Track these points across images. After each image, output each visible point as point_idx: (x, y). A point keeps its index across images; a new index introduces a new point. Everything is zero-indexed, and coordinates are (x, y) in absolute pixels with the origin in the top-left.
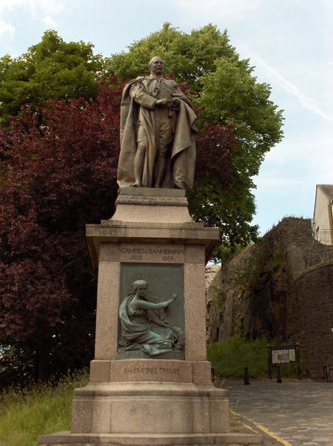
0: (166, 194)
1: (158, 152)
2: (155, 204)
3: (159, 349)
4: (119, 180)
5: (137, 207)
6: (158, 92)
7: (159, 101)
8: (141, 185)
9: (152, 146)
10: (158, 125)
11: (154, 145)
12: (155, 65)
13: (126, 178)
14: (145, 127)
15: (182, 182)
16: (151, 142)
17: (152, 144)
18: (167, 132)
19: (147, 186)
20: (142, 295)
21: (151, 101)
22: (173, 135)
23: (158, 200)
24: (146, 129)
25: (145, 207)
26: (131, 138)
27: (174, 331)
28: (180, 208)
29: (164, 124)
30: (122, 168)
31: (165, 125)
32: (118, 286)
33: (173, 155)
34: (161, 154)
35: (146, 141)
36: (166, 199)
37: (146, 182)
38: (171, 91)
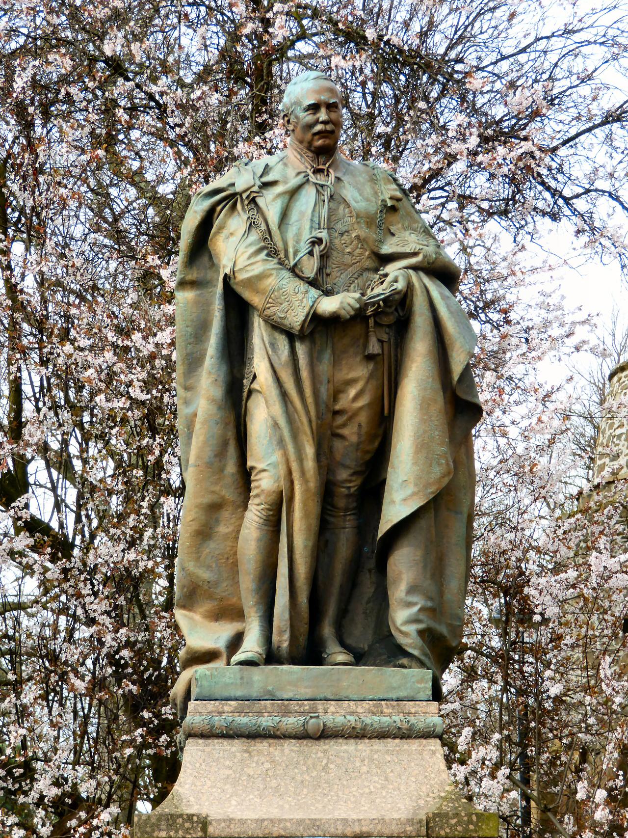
0: (346, 687)
1: (327, 492)
2: (325, 734)
4: (184, 607)
5: (263, 746)
6: (324, 257)
7: (329, 305)
8: (271, 657)
9: (306, 491)
11: (312, 485)
12: (309, 118)
14: (277, 409)
15: (421, 633)
16: (303, 473)
17: (305, 481)
18: (363, 418)
19: (294, 660)
20: (199, 591)
21: (298, 303)
23: (335, 715)
24: (282, 422)
25: (290, 747)
26: (225, 444)
28: (414, 745)
30: (191, 566)
31: (352, 392)
33: (384, 526)
34: (341, 503)
35: (282, 470)
36: (363, 714)
37: (286, 636)
38: (372, 235)
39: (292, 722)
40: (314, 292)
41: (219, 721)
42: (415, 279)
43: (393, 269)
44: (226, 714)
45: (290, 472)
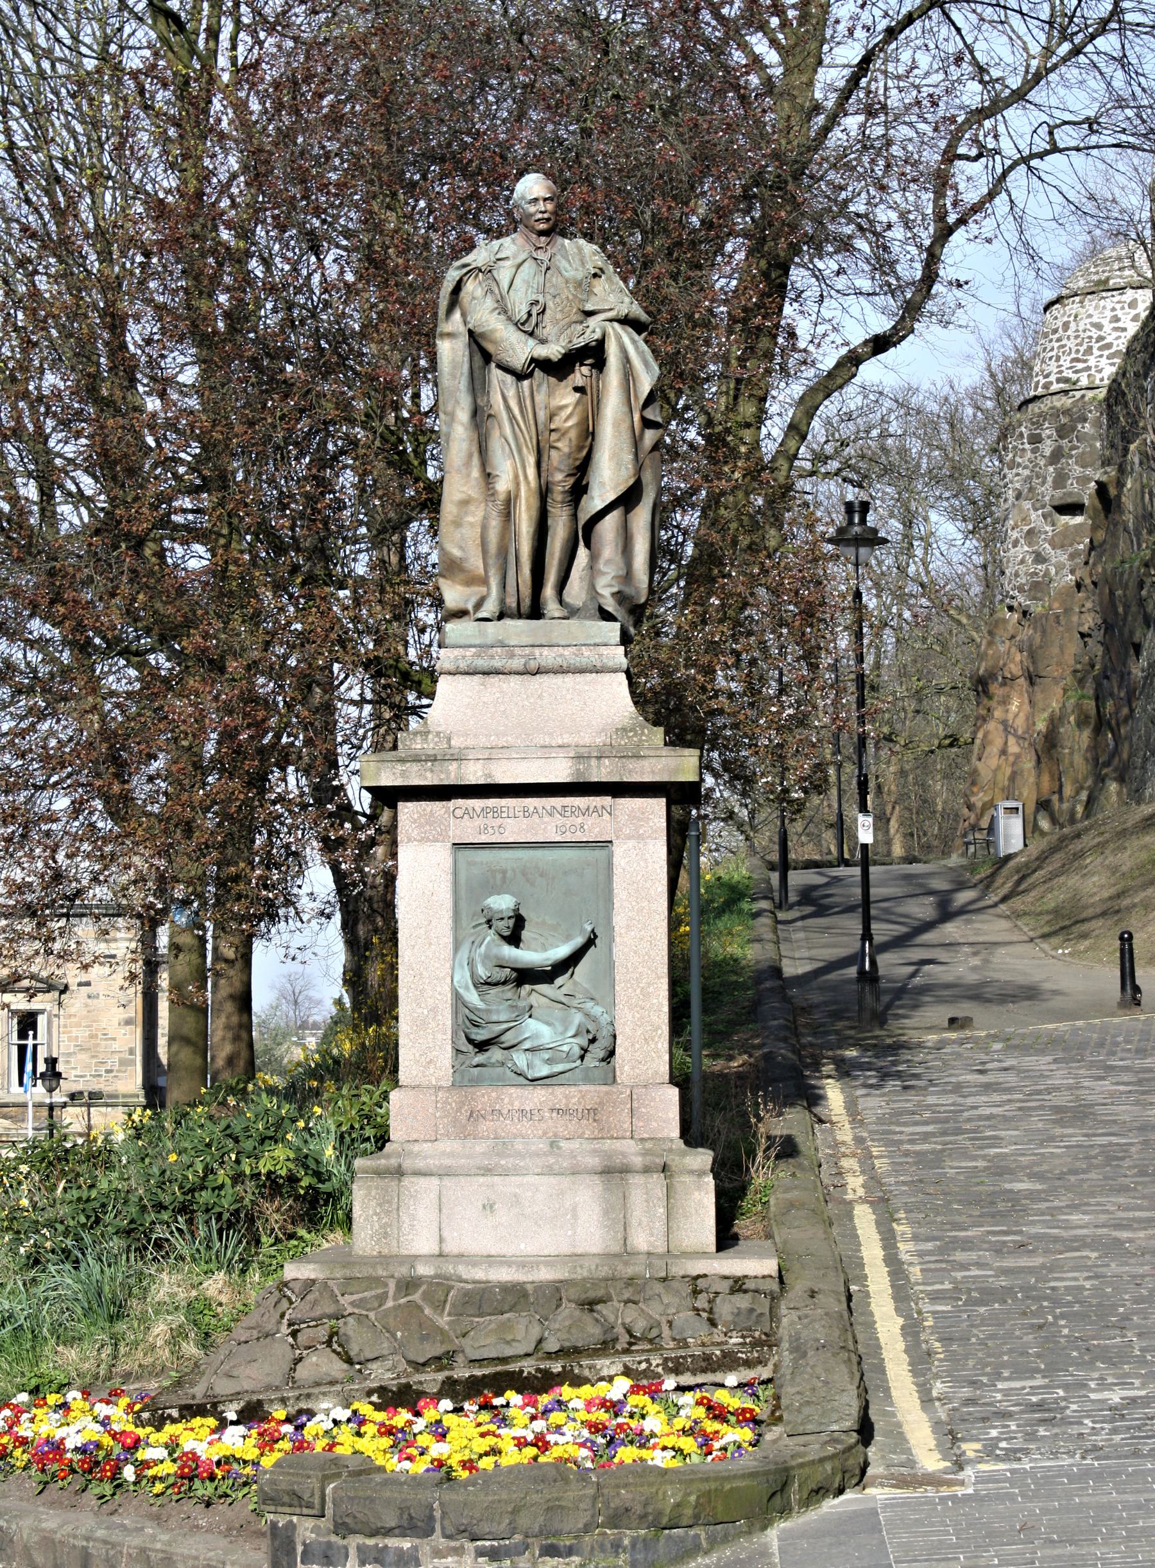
1: (544, 494)
3: (549, 1061)
5: (494, 680)
10: (542, 415)
13: (461, 576)
18: (573, 434)
19: (520, 615)
22: (588, 435)
23: (547, 657)
25: (515, 680)
26: (470, 456)
27: (587, 1015)
29: (562, 408)
31: (564, 414)
32: (448, 904)
36: (568, 656)
39: (517, 663)
40: (531, 342)
41: (463, 665)
42: (610, 330)
43: (593, 322)
44: (467, 657)
45: (516, 477)
